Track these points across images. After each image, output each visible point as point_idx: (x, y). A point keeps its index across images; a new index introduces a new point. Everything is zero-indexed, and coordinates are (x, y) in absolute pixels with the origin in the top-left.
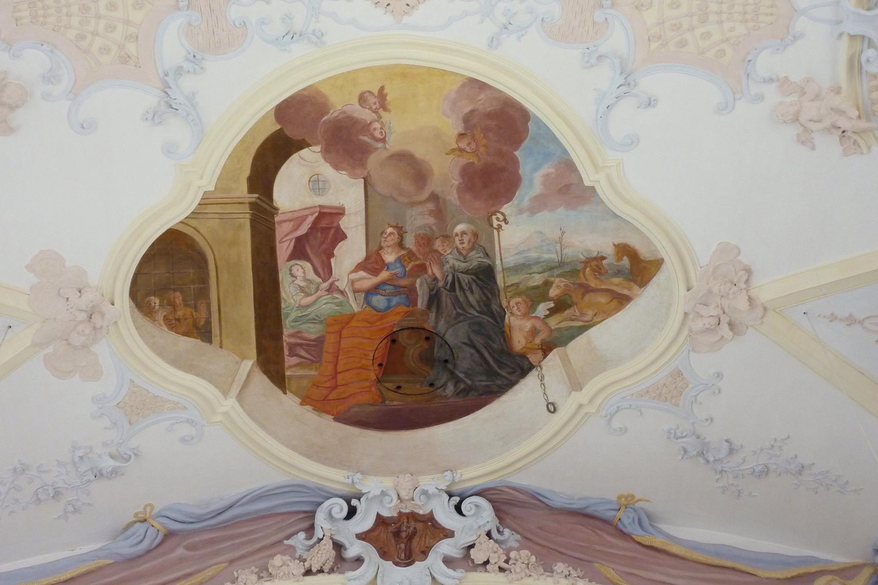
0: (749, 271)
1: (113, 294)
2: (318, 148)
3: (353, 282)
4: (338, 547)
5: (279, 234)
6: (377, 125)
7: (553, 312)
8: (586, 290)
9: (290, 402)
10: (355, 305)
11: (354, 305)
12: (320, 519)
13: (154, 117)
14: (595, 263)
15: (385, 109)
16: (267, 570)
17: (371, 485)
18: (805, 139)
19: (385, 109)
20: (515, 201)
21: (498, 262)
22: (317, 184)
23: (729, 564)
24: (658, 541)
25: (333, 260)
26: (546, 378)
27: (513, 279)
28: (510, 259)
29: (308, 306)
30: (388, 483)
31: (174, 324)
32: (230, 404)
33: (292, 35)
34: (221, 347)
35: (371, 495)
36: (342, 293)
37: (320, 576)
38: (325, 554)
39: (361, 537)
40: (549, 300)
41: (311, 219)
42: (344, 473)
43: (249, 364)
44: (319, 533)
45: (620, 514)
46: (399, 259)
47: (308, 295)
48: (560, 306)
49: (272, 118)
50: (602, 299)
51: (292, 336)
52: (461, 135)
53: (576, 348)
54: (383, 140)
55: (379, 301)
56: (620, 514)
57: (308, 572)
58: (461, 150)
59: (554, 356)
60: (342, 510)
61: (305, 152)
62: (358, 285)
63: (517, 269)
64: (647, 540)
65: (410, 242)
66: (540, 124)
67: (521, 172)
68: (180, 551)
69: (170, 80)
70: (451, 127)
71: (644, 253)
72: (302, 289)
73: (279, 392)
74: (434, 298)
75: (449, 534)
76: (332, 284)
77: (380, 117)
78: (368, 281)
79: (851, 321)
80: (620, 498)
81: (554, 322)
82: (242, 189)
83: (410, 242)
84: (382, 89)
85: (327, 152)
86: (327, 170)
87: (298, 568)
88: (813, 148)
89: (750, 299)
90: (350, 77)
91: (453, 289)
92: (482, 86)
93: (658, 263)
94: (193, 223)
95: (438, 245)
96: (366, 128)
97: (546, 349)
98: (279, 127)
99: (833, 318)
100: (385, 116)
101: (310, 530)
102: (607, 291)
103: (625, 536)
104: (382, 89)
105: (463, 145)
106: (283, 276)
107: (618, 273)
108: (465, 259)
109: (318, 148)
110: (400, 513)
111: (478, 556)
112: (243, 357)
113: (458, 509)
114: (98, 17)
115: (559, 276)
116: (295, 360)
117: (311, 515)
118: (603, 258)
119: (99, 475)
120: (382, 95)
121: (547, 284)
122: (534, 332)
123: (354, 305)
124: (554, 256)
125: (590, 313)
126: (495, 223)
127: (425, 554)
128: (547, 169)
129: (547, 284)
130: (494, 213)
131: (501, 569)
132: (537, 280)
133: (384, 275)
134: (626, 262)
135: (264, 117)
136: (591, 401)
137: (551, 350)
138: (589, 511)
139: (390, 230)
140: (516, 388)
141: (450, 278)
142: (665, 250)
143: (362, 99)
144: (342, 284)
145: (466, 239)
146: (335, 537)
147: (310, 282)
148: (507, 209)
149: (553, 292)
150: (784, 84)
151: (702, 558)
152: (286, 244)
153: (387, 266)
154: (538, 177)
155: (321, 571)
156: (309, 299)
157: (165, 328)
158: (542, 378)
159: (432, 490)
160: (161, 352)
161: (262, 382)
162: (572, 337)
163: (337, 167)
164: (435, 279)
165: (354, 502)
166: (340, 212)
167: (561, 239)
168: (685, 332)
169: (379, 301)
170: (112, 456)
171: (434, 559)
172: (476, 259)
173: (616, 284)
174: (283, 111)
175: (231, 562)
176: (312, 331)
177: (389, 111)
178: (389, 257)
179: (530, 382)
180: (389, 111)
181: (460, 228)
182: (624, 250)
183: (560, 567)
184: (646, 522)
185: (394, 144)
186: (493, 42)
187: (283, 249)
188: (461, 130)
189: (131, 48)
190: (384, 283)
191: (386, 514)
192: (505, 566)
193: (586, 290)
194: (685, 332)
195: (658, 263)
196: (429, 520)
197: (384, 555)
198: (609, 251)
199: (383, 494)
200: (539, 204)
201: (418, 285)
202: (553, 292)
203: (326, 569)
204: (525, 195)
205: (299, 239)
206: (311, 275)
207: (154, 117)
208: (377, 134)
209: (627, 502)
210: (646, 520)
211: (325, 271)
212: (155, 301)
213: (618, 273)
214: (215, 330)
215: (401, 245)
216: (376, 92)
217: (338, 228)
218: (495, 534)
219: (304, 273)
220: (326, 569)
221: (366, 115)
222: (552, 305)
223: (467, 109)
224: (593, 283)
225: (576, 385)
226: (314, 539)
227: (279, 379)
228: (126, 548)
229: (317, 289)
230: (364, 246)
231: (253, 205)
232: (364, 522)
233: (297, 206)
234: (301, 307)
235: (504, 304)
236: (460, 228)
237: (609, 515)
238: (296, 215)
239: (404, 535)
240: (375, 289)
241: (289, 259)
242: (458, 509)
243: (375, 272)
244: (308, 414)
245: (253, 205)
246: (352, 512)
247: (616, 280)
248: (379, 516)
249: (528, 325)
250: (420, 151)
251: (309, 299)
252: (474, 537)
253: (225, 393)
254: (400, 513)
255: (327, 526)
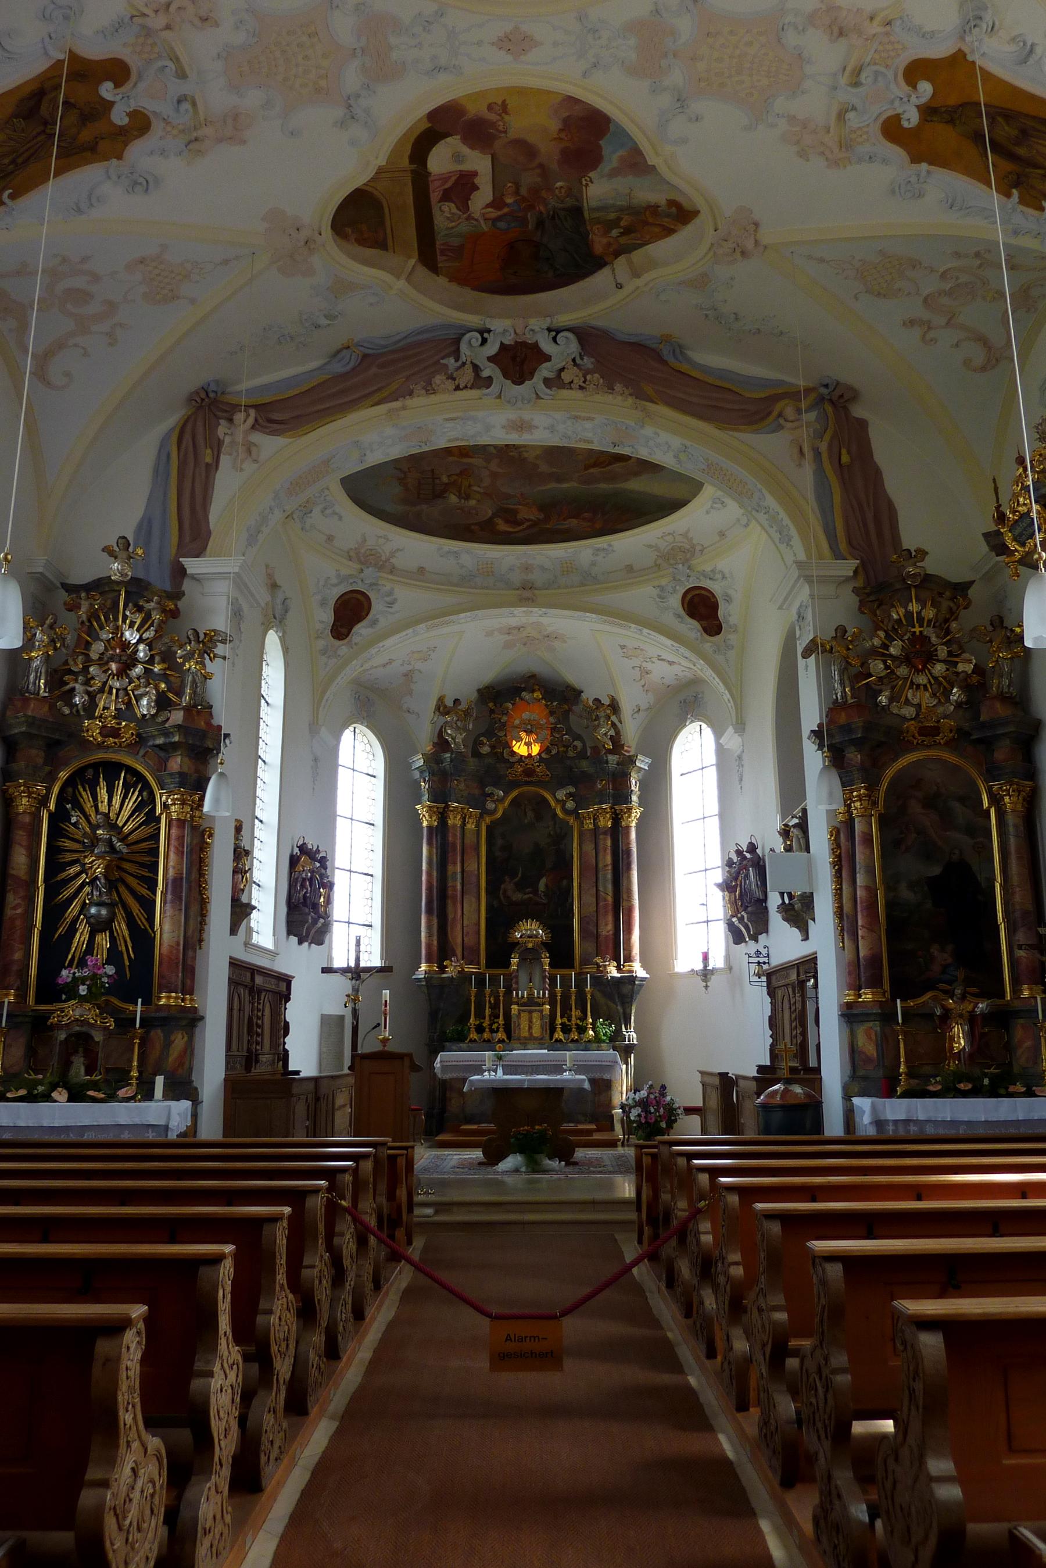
0: (756, 225)
1: (320, 227)
2: (459, 137)
3: (484, 214)
4: (476, 368)
5: (432, 186)
6: (501, 123)
7: (622, 234)
8: (646, 223)
9: (442, 281)
10: (485, 227)
11: (484, 226)
12: (464, 347)
13: (342, 124)
14: (653, 209)
15: (507, 113)
16: (431, 384)
17: (497, 325)
18: (803, 154)
19: (507, 113)
20: (599, 170)
21: (585, 204)
22: (457, 158)
23: (727, 385)
24: (684, 367)
25: (470, 202)
26: (616, 270)
27: (596, 215)
28: (594, 204)
29: (452, 228)
30: (508, 323)
31: (362, 242)
32: (401, 284)
33: (439, 69)
34: (394, 252)
35: (497, 332)
36: (476, 220)
37: (465, 391)
38: (468, 374)
39: (490, 359)
40: (621, 227)
41: (453, 179)
42: (480, 317)
43: (412, 262)
44: (463, 359)
45: (661, 346)
46: (515, 202)
47: (453, 222)
48: (628, 231)
49: (425, 120)
50: (657, 230)
51: (443, 244)
52: (561, 130)
53: (637, 255)
54: (505, 132)
55: (502, 225)
56: (661, 346)
57: (457, 388)
58: (561, 139)
59: (622, 260)
60: (477, 339)
61: (449, 139)
62: (488, 216)
63: (598, 209)
64: (676, 365)
65: (524, 191)
66: (618, 126)
67: (603, 153)
68: (374, 370)
69: (352, 102)
70: (554, 125)
71: (686, 205)
72: (448, 218)
73: (434, 276)
74: (540, 224)
75: (548, 358)
76: (469, 216)
77: (503, 118)
78: (494, 213)
79: (821, 260)
80: (662, 336)
81: (623, 240)
82: (405, 163)
83: (524, 191)
84: (504, 101)
85: (465, 140)
86: (465, 150)
87: (450, 385)
88: (808, 160)
89: (756, 241)
90: (481, 94)
91: (553, 218)
92: (578, 101)
93: (696, 213)
94: (371, 184)
95: (544, 194)
96: (493, 124)
97: (617, 254)
98: (430, 125)
99: (810, 257)
100: (506, 118)
101: (457, 356)
102: (659, 225)
103: (665, 363)
104: (504, 101)
105: (563, 135)
106: (435, 211)
107: (668, 216)
108: (562, 202)
109: (459, 137)
110: (516, 342)
111: (566, 377)
112: (409, 257)
113: (554, 339)
114: (297, 65)
115: (628, 214)
116: (445, 258)
117: (457, 341)
118: (659, 207)
119: (317, 327)
120: (504, 105)
121: (619, 219)
122: (609, 244)
123: (484, 226)
124: (624, 203)
125: (648, 237)
126: (584, 182)
127: (531, 375)
128: (621, 153)
129: (619, 219)
130: (584, 176)
131: (581, 388)
132: (613, 216)
133: (506, 210)
134: (674, 210)
135: (421, 118)
136: (646, 285)
137: (620, 255)
138: (642, 343)
139: (510, 185)
140: (596, 275)
141: (551, 213)
142: (700, 204)
143: (490, 107)
144: (477, 215)
145: (563, 191)
146: (474, 361)
147: (453, 214)
148: (592, 174)
149: (623, 223)
150: (792, 119)
151: (710, 380)
152: (436, 194)
153: (507, 205)
154: (615, 158)
155: (466, 387)
156: (453, 224)
157: (356, 245)
158: (613, 270)
159: (537, 328)
160: (355, 258)
161: (422, 272)
162: (636, 249)
163: (472, 148)
164: (541, 213)
165: (486, 335)
166: (475, 174)
167: (630, 194)
168: (711, 253)
169: (502, 225)
170: (326, 316)
171: (537, 379)
172: (569, 202)
173: (666, 222)
174: (432, 115)
175: (408, 378)
176: (456, 242)
177: (509, 115)
178: (509, 200)
179: (606, 272)
180: (509, 115)
181: (559, 184)
182: (672, 203)
183: (618, 387)
184: (678, 351)
185: (512, 134)
186: (585, 74)
187: (435, 196)
188: (561, 126)
189: (323, 83)
190: (505, 215)
191: (507, 342)
192: (583, 385)
193: (646, 223)
194: (711, 253)
195: (696, 213)
196: (535, 347)
197: (506, 376)
198: (663, 202)
199: (505, 331)
200: (615, 173)
201: (529, 216)
202: (623, 223)
203: (469, 386)
204: (606, 167)
205: (445, 190)
206: (454, 210)
207: (342, 124)
208: (501, 128)
209: (666, 339)
210: (679, 350)
211: (464, 207)
212: (349, 230)
213: (668, 216)
214: (390, 243)
215: (517, 192)
216: (500, 103)
217: (473, 184)
218: (578, 361)
219: (450, 209)
220: (469, 386)
221: (492, 117)
222: (622, 230)
223: (567, 114)
224: (651, 220)
225: (637, 275)
226: (460, 363)
227: (433, 267)
228: (338, 368)
229: (459, 218)
230: (491, 193)
231: (412, 172)
232: (492, 349)
233: (444, 170)
234: (448, 228)
235: (589, 228)
236: (559, 184)
237: (654, 346)
238: (444, 176)
239: (518, 359)
240: (499, 219)
241: (439, 202)
242: (554, 339)
243: (499, 209)
244: (454, 287)
245: (412, 172)
246: (484, 341)
247: (666, 219)
248: (502, 343)
249: (605, 241)
250: (531, 139)
251: (453, 224)
252: (564, 363)
253: (398, 277)
254: (516, 342)
255: (468, 353)
